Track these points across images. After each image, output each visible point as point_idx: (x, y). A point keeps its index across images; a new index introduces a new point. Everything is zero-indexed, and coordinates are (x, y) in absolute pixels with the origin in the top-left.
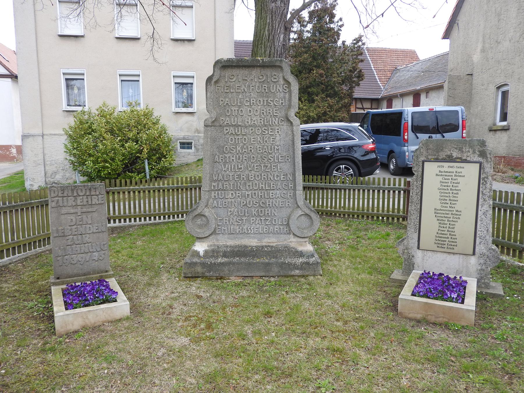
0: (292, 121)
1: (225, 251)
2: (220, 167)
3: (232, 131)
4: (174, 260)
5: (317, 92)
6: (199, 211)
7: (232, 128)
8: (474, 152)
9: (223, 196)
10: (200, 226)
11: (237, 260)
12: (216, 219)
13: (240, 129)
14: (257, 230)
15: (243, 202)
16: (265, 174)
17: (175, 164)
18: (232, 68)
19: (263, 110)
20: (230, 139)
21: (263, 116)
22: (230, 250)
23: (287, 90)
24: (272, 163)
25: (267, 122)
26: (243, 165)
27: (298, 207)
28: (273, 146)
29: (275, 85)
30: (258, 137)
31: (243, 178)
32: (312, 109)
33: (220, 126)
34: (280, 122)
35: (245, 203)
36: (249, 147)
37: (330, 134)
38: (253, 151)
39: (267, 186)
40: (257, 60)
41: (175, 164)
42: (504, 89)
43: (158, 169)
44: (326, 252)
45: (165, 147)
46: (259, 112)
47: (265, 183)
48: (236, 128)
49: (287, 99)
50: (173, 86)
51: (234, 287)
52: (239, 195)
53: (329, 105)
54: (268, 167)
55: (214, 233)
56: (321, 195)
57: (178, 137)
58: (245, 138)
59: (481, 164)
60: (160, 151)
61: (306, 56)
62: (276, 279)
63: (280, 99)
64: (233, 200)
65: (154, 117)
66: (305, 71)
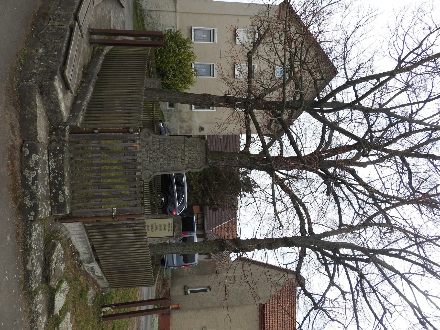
6: (151, 134)
8: (177, 234)
10: (145, 134)
42: (208, 290)
59: (173, 236)
65: (188, 85)
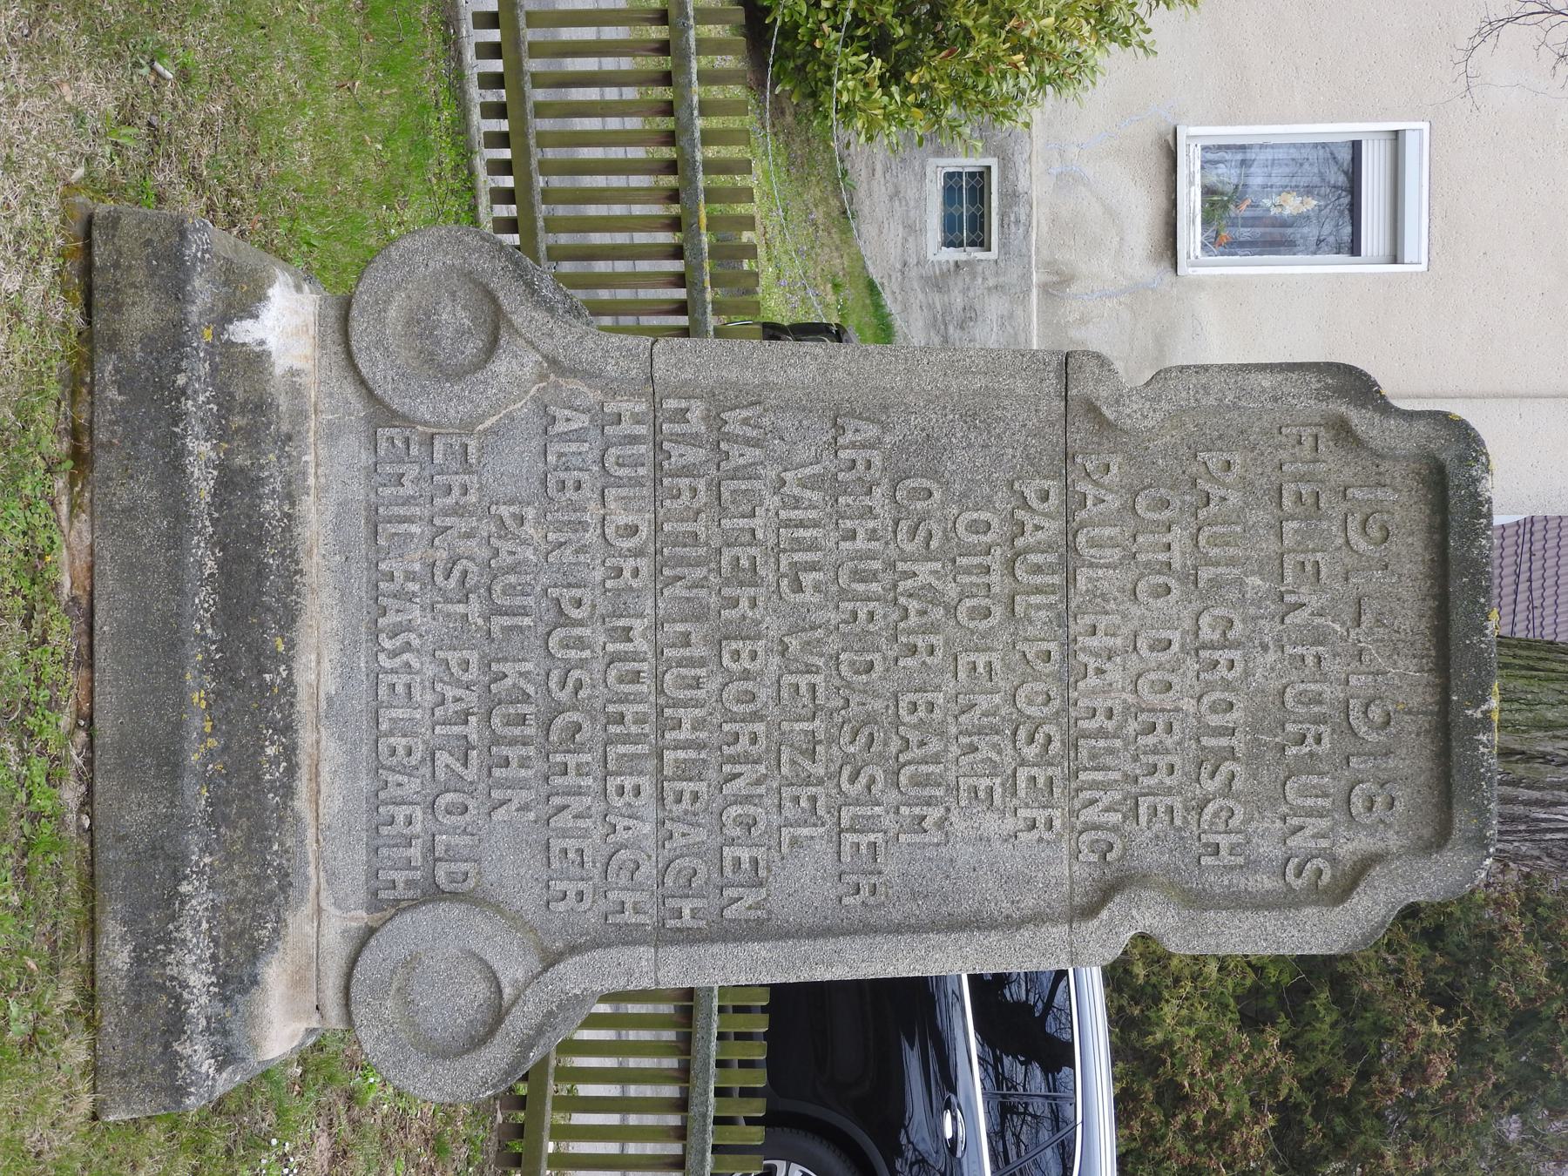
0: (1104, 914)
1: (260, 481)
2: (803, 453)
3: (1038, 528)
4: (205, 152)
5: (1311, 1046)
6: (522, 314)
7: (1053, 527)
9: (622, 472)
10: (421, 325)
11: (201, 565)
12: (467, 427)
13: (1049, 580)
14: (400, 689)
15: (579, 603)
16: (762, 741)
17: (849, 138)
18: (1431, 529)
19: (1169, 729)
20: (985, 516)
21: (1132, 727)
22: (266, 516)
23: (1297, 884)
24: (831, 784)
25: (1093, 757)
26: (817, 598)
27: (551, 960)
28: (939, 792)
29: (1327, 803)
30: (997, 699)
31: (735, 603)
32: (1201, 1014)
33: (1068, 456)
34: (1093, 835)
35: (575, 614)
36: (933, 639)
37: (1045, 1135)
38: (910, 662)
39: (681, 754)
40: (1486, 688)
41: (849, 138)
43: (814, 34)
44: (257, 1143)
45: (954, 81)
46: (1155, 700)
47: (700, 746)
48: (1052, 558)
49: (1240, 882)
50: (1339, 130)
51: (21, 541)
52: (627, 574)
53: (1231, 1126)
54: (807, 764)
55: (380, 412)
56: (648, 1091)
57: (1018, 159)
58: (988, 614)
60: (929, 42)
61: (1537, 969)
62: (71, 817)
63: (1240, 838)
64: (591, 536)
66: (1443, 969)
